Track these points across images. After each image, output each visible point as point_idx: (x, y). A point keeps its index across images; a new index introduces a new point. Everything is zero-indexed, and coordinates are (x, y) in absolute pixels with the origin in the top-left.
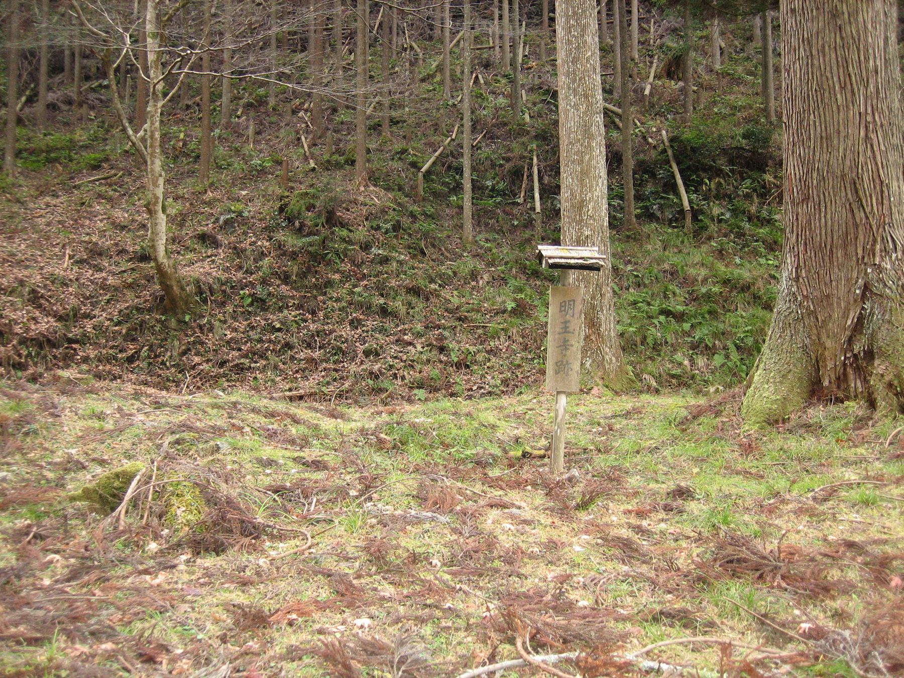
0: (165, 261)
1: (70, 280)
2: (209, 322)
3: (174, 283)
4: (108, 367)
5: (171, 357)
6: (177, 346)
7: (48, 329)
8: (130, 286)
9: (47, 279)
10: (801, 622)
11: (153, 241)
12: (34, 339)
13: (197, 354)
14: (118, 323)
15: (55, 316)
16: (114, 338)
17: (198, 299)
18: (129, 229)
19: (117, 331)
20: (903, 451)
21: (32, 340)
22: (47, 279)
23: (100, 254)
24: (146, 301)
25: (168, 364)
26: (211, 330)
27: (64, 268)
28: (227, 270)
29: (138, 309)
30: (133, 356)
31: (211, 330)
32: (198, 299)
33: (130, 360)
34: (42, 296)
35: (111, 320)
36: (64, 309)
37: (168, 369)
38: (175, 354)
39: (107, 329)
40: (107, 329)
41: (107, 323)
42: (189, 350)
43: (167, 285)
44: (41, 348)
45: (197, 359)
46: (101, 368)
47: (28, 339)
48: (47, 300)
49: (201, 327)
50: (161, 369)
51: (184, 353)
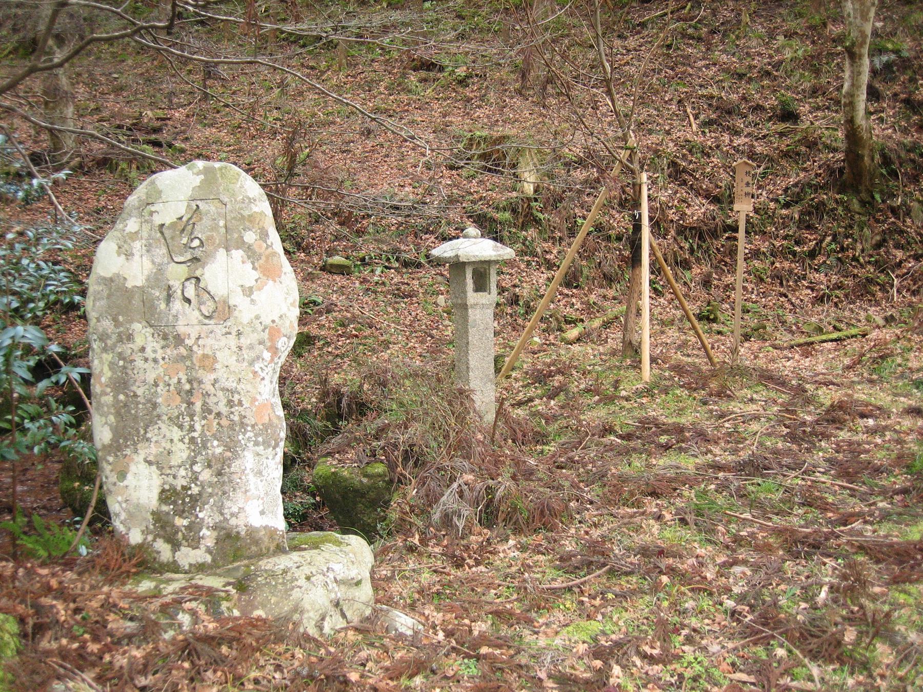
0: (863, 123)
1: (710, 148)
2: (904, 204)
3: (866, 152)
4: (786, 265)
5: (863, 251)
6: (871, 236)
7: (704, 213)
8: (786, 155)
9: (683, 147)
10: (905, 491)
11: (852, 96)
12: (694, 228)
13: (898, 246)
14: (787, 205)
15: (706, 197)
16: (785, 226)
17: (884, 171)
18: (750, 79)
19: (787, 216)
20: (918, 284)
21: (691, 228)
22: (683, 147)
23: (729, 113)
24: (817, 175)
25: (862, 260)
26: (908, 213)
27: (692, 132)
28: (905, 131)
29: (810, 186)
30: (814, 250)
31: (908, 213)
32: (884, 171)
33: (812, 254)
34: (684, 171)
35: (777, 201)
36: (717, 186)
37: (862, 266)
38: (867, 246)
39: (774, 213)
40: (774, 213)
41: (772, 205)
42: (884, 240)
43: (858, 155)
44: (701, 238)
45: (899, 254)
46: (777, 265)
47: (686, 228)
48: (692, 175)
49: (894, 211)
50: (854, 267)
51: (878, 246)
